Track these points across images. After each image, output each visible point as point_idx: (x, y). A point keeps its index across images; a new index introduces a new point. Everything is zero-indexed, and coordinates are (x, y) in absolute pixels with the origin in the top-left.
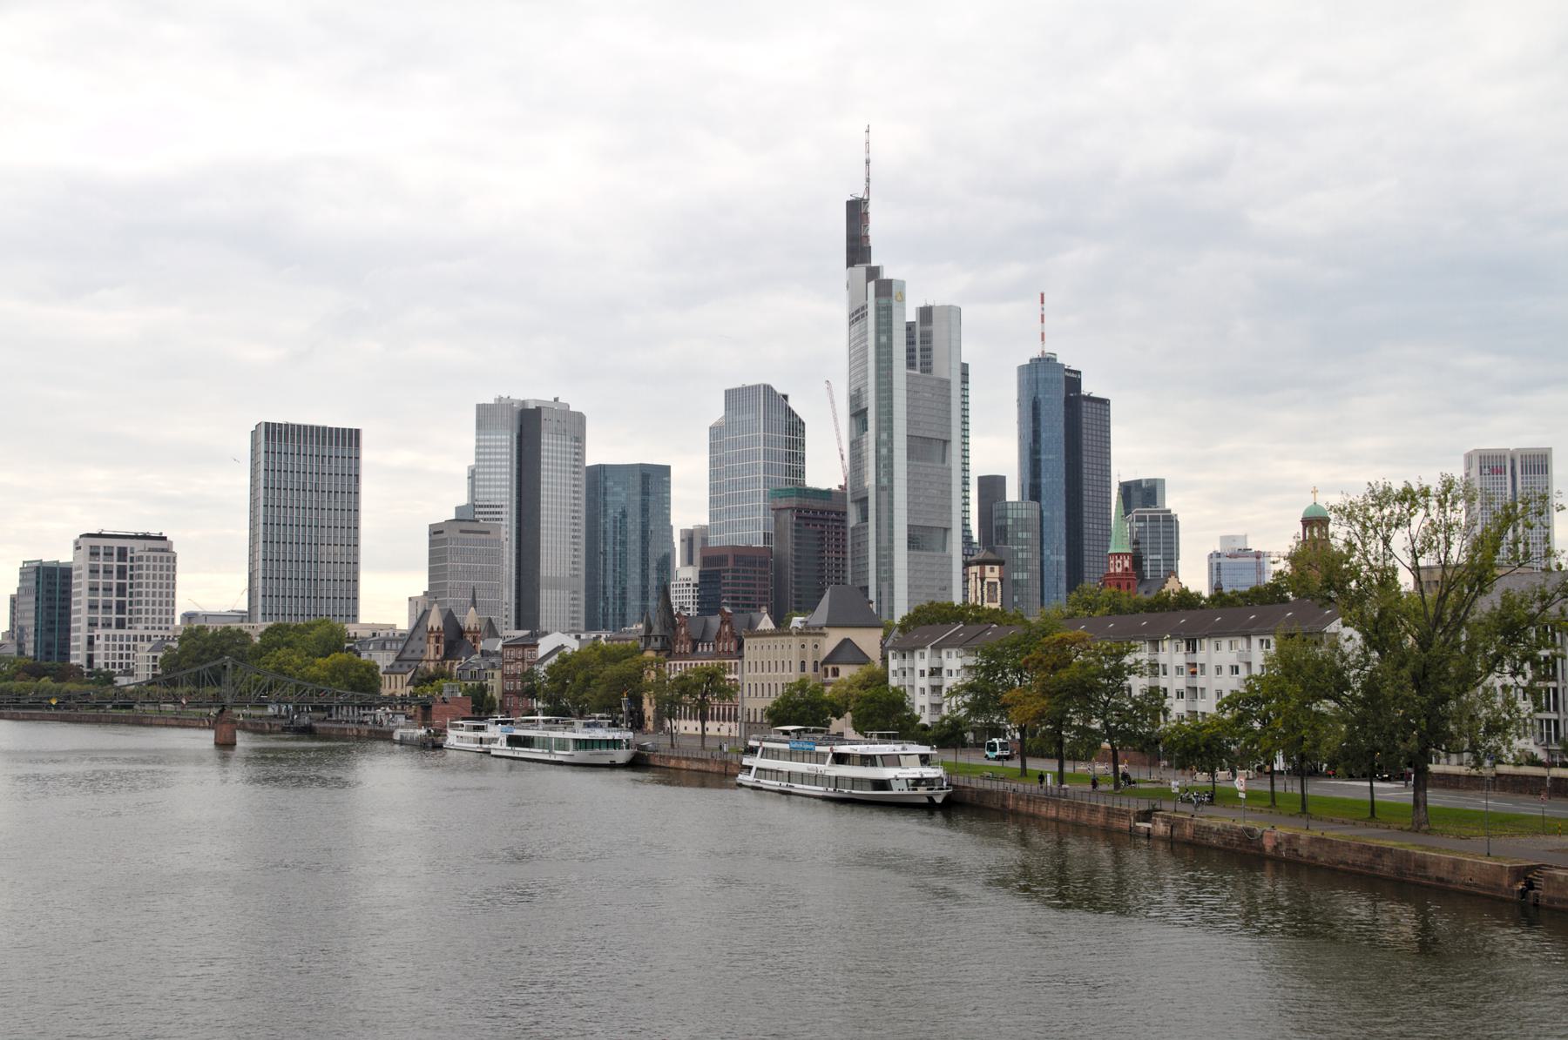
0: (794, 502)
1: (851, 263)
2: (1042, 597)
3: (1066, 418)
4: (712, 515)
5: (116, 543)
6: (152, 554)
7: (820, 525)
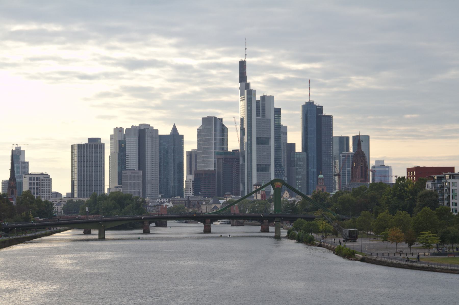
0: (223, 156)
1: (241, 81)
4: (199, 145)
5: (36, 176)
6: (46, 179)
7: (232, 160)
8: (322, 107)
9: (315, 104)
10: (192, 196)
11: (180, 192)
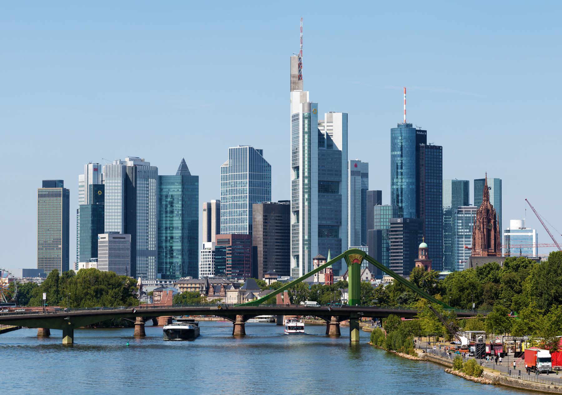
8: (426, 131)
9: (414, 127)
10: (212, 276)
11: (191, 269)
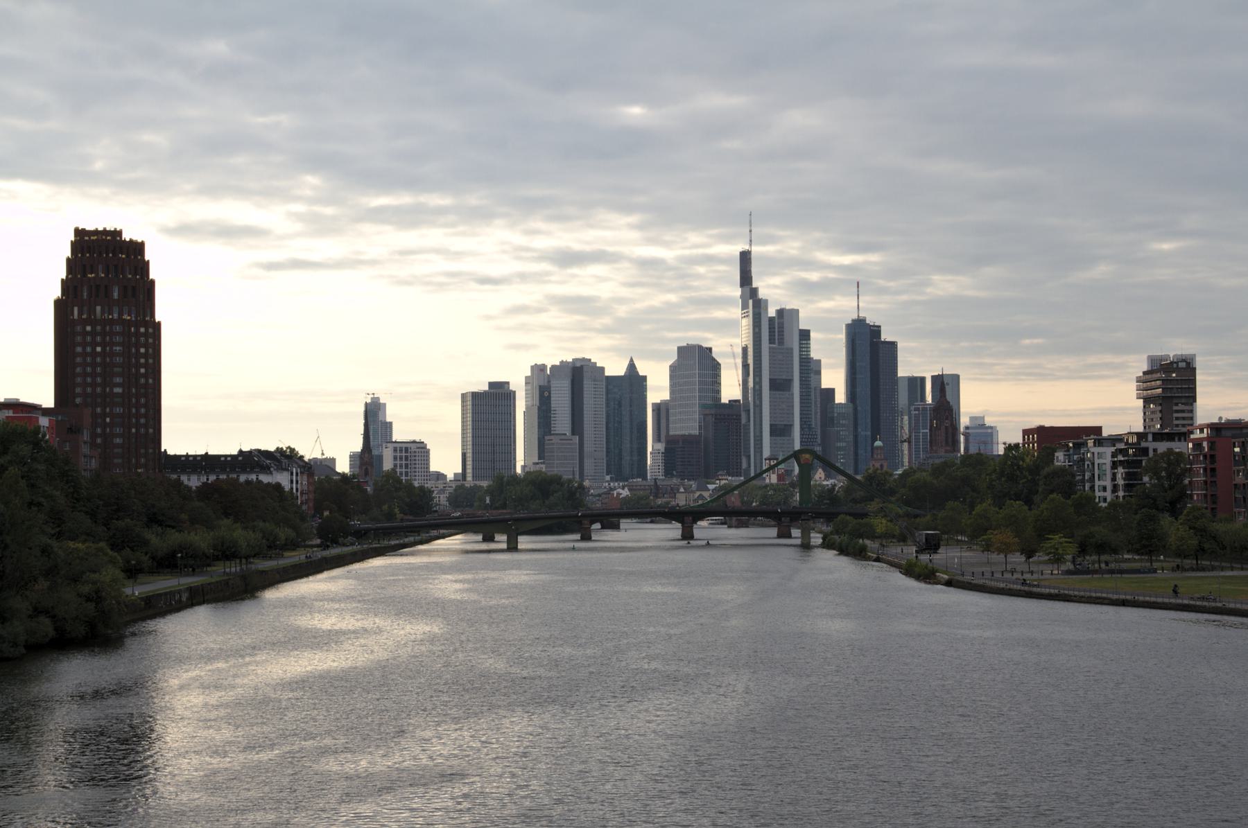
1: (742, 286)
2: (856, 454)
3: (869, 349)
7: (728, 418)
